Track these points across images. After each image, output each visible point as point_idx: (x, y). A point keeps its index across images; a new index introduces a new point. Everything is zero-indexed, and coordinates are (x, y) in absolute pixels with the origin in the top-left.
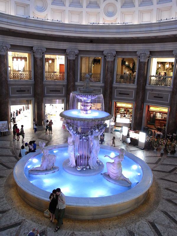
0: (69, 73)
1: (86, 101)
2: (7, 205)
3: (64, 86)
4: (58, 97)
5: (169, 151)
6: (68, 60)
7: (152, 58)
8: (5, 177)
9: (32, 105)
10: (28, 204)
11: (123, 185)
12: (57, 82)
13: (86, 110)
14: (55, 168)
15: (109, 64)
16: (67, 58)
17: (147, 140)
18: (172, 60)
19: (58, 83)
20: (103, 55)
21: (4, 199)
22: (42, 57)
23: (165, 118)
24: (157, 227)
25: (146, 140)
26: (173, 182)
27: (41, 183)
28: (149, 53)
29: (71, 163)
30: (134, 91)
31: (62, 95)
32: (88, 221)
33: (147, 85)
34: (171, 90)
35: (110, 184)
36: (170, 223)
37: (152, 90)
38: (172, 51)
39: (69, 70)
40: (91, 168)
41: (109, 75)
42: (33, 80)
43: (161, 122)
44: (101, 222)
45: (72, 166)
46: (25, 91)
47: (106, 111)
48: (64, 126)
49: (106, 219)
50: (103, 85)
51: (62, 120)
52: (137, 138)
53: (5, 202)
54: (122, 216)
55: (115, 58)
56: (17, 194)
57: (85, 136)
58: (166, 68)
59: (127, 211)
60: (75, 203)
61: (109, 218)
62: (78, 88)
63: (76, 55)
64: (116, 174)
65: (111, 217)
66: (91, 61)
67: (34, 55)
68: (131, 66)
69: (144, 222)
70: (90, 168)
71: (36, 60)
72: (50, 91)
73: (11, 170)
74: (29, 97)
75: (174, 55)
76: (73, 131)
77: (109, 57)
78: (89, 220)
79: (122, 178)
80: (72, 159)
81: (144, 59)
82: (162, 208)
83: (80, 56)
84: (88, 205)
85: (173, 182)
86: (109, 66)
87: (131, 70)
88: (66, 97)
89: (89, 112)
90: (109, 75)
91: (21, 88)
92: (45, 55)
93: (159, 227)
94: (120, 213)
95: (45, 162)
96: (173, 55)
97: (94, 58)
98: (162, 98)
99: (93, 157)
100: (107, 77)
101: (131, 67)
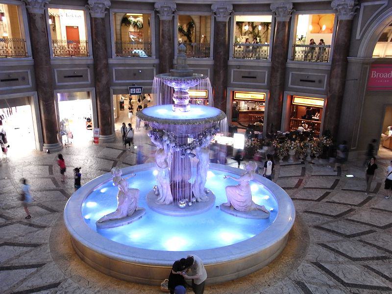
0: (96, 43)
1: (183, 90)
2: (84, 291)
3: (88, 66)
4: (80, 87)
5: (282, 158)
6: (91, 18)
7: (296, 16)
8: (44, 243)
9: (33, 106)
10: (121, 280)
11: (258, 217)
12: (75, 59)
13: (185, 106)
14: (139, 210)
15: (166, 25)
16: (90, 16)
17: (247, 146)
18: (268, 19)
19: (77, 62)
20: (211, 10)
21: (70, 281)
22: (43, 13)
23: (253, 109)
24: (325, 266)
25: (245, 146)
26: (308, 200)
27: (125, 237)
28: (232, 8)
29: (164, 198)
30: (209, 71)
31: (87, 84)
32: (233, 281)
33: (288, 61)
34: (269, 65)
35: (239, 220)
36: (337, 257)
37: (239, 67)
38: (269, 5)
39: (97, 37)
40: (199, 200)
41: (166, 44)
42: (92, 57)
43: (250, 116)
44: (250, 278)
45: (167, 202)
46: (17, 79)
47: (215, 105)
48: (96, 140)
49: (255, 273)
50: (156, 61)
51: (90, 128)
52: (230, 144)
53: (76, 285)
54: (274, 263)
55: (173, 15)
56: (88, 268)
57: (190, 148)
58: (244, 31)
59: (278, 253)
60: (213, 258)
61: (258, 270)
62: (114, 70)
63: (106, 9)
64: (245, 202)
65: (261, 269)
66: (120, 21)
67: (27, 10)
68: (185, 29)
69: (306, 264)
70: (197, 201)
71: (34, 18)
72: (65, 77)
73: (46, 229)
74: (28, 90)
75: (273, 11)
76: (168, 142)
77: (282, 14)
78: (233, 281)
79: (253, 207)
80: (165, 191)
81: (223, 17)
82: (316, 240)
83: (112, 12)
84: (234, 256)
85: (308, 200)
86: (166, 29)
87: (185, 35)
88: (37, 91)
89: (189, 107)
90: (166, 44)
91: (9, 75)
92: (49, 9)
93: (327, 266)
94: (270, 260)
95: (126, 202)
96: (332, 9)
97: (123, 14)
98: (256, 78)
99: (200, 182)
100: (163, 48)
101: (186, 31)
